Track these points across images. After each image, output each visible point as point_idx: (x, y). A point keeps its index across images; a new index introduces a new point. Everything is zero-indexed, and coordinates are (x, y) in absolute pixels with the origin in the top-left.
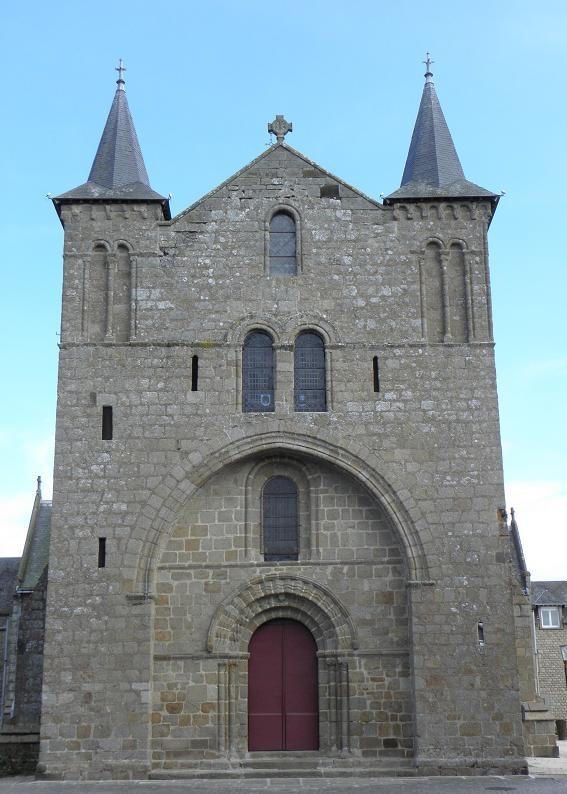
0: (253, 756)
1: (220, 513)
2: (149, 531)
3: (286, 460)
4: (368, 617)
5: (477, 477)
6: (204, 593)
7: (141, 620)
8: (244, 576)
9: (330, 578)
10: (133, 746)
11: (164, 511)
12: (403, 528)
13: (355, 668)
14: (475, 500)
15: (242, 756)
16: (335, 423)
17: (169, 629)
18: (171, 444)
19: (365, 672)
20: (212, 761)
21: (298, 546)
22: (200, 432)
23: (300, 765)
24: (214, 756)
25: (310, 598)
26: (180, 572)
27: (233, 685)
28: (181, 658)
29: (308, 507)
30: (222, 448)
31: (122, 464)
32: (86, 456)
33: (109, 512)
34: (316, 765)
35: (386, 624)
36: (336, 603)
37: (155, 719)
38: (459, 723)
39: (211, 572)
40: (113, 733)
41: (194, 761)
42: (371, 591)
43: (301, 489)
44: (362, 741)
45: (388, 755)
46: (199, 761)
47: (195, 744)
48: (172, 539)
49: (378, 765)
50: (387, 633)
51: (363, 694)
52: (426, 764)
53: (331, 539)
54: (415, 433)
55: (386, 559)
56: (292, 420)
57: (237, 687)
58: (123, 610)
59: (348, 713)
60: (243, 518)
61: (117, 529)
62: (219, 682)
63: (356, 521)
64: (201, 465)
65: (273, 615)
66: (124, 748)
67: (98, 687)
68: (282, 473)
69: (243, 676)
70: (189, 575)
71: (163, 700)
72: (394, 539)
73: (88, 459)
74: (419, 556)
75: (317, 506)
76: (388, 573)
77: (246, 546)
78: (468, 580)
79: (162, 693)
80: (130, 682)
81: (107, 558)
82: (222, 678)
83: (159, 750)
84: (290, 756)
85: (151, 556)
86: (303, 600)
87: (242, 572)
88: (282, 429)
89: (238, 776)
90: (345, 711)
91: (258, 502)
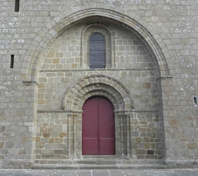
0: (84, 158)
1: (69, 47)
2: (34, 52)
3: (100, 25)
4: (139, 94)
5: (191, 29)
6: (61, 82)
7: (30, 93)
8: (80, 75)
9: (120, 76)
10: (24, 152)
11: (42, 43)
12: (156, 52)
13: (133, 117)
14: (190, 39)
15: (79, 158)
16: (123, 4)
17: (45, 99)
18: (46, 13)
19: (138, 120)
20: (64, 160)
21: (105, 63)
22: (59, 8)
23: (107, 163)
24: (65, 158)
25: (111, 85)
26: (50, 72)
27: (75, 125)
28: (50, 112)
29: (110, 46)
30: (70, 15)
31: (23, 22)
32: (6, 19)
33: (16, 43)
34: (115, 163)
35: (147, 97)
36: (123, 87)
37: (37, 140)
38: (186, 143)
39: (65, 73)
40: (15, 146)
41: (55, 160)
42: (140, 82)
43: (107, 38)
44: (136, 151)
45: (149, 158)
46: (58, 160)
47: (56, 152)
48: (47, 58)
49: (144, 163)
50: (148, 102)
51: (137, 129)
52: (170, 163)
53: (121, 59)
54: (161, 9)
55: (147, 68)
56: (103, 3)
57: (77, 126)
58: (20, 88)
59: (130, 138)
60: (80, 50)
61: (19, 51)
62: (68, 123)
63: (132, 51)
64: (60, 23)
65: (94, 94)
66: (20, 153)
67: (8, 124)
68: (98, 31)
69: (80, 121)
70: (54, 75)
71: (41, 131)
72: (150, 59)
73: (7, 20)
74: (164, 65)
75: (114, 44)
76: (148, 74)
77: (81, 62)
78: (188, 75)
79: (41, 128)
80: (23, 122)
81: (14, 64)
82: (70, 122)
83: (39, 154)
84: (102, 158)
85: (35, 63)
86: (108, 86)
87: (79, 73)
88: (98, 7)
89: (76, 168)
90: (128, 137)
91: (87, 44)
